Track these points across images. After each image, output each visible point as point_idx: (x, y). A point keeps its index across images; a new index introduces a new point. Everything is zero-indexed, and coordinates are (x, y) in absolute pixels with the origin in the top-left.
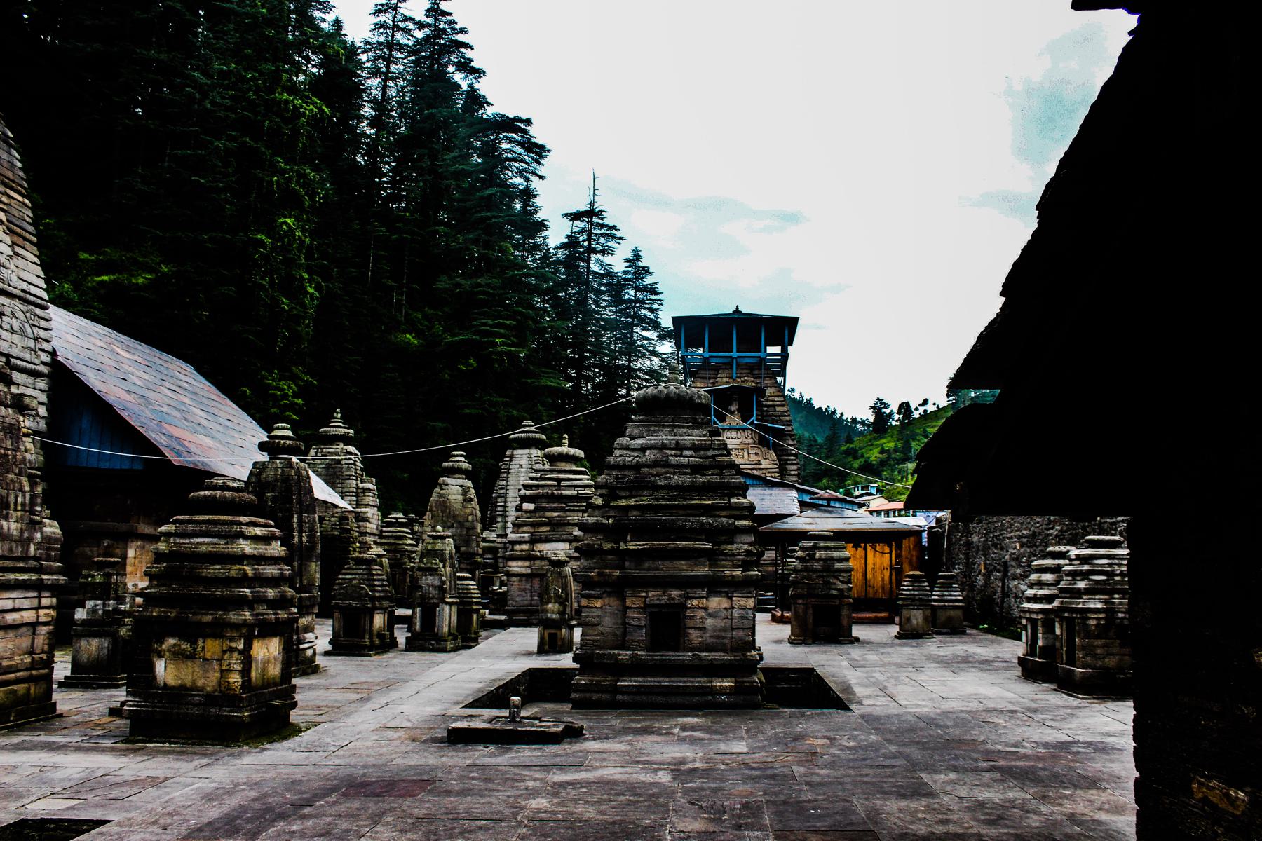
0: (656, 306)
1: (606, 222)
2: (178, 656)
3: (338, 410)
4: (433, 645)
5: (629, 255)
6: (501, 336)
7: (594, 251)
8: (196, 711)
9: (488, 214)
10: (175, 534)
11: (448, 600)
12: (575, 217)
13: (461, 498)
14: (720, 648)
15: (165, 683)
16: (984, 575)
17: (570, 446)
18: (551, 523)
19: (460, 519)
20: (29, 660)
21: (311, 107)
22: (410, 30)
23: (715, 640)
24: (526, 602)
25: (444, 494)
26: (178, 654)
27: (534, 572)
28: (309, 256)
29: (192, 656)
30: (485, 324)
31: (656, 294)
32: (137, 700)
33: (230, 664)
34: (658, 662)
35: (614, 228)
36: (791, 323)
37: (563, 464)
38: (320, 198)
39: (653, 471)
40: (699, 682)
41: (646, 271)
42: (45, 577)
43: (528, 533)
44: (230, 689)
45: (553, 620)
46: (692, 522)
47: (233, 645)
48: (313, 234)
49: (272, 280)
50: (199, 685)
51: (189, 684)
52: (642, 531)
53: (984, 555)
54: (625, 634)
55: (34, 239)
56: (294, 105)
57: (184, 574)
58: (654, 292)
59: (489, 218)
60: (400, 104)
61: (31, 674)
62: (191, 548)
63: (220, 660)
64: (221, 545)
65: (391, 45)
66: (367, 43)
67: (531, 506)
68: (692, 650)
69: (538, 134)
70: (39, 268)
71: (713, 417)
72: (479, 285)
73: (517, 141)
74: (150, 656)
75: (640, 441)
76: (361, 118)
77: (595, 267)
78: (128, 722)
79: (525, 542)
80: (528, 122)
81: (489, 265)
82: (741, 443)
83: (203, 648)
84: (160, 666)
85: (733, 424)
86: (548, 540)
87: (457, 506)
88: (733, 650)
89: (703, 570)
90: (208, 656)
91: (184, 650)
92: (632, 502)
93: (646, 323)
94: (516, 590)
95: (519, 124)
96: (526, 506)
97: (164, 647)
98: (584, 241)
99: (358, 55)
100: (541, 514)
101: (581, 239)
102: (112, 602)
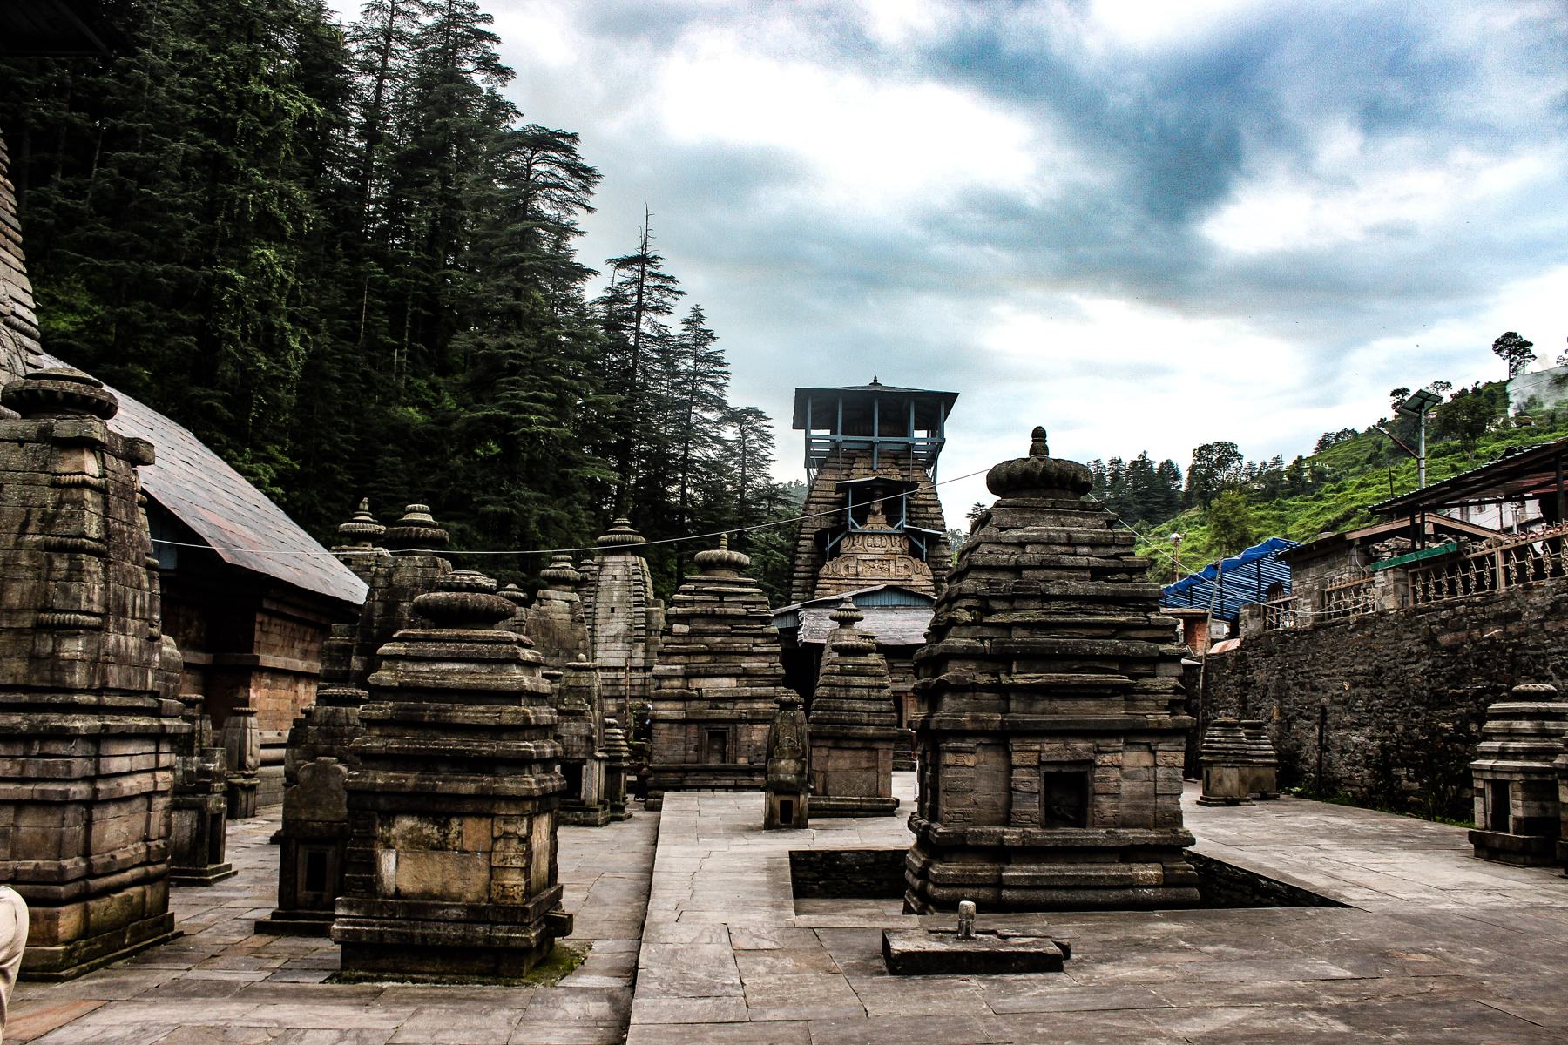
0: (721, 381)
1: (661, 271)
2: (417, 844)
3: (366, 499)
4: (577, 816)
5: (688, 315)
6: (538, 412)
7: (645, 308)
8: (452, 931)
9: (522, 255)
10: (406, 658)
11: (599, 755)
12: (623, 263)
13: (568, 617)
14: (1139, 821)
15: (397, 889)
16: (1278, 723)
17: (730, 548)
18: (714, 653)
19: (568, 646)
20: (143, 850)
21: (298, 104)
22: (415, 14)
23: (1133, 812)
24: (678, 758)
25: (545, 612)
26: (418, 844)
27: (690, 717)
28: (293, 298)
29: (441, 847)
30: (514, 397)
31: (722, 365)
32: (353, 914)
33: (505, 858)
34: (1060, 844)
35: (672, 279)
36: (947, 400)
37: (724, 572)
38: (309, 225)
39: (1041, 574)
40: (1117, 870)
41: (708, 335)
42: (166, 722)
43: (680, 664)
44: (506, 897)
45: (788, 783)
46: (1103, 646)
47: (510, 828)
48: (301, 271)
49: (244, 329)
50: (453, 890)
51: (436, 890)
52: (1034, 658)
53: (1280, 698)
54: (1009, 804)
55: (20, 238)
56: (276, 102)
57: (426, 719)
58: (719, 362)
59: (523, 260)
60: (403, 109)
61: (147, 873)
62: (434, 679)
63: (489, 853)
64: (483, 676)
65: (388, 34)
66: (358, 28)
67: (685, 629)
68: (1104, 825)
69: (587, 154)
70: (26, 279)
71: (851, 519)
72: (509, 346)
73: (560, 162)
74: (372, 846)
75: (1014, 533)
76: (346, 126)
77: (646, 328)
78: (339, 947)
79: (677, 677)
80: (574, 137)
81: (515, 318)
82: (887, 553)
83: (460, 833)
84: (388, 863)
85: (877, 529)
86: (708, 675)
87: (564, 628)
88: (1157, 825)
89: (1116, 713)
90: (468, 846)
91: (427, 836)
92: (1014, 617)
93: (707, 401)
94: (665, 741)
95: (561, 140)
96: (677, 628)
97: (394, 831)
98: (633, 295)
99: (345, 43)
100: (698, 639)
101: (629, 292)
102: (195, 758)
